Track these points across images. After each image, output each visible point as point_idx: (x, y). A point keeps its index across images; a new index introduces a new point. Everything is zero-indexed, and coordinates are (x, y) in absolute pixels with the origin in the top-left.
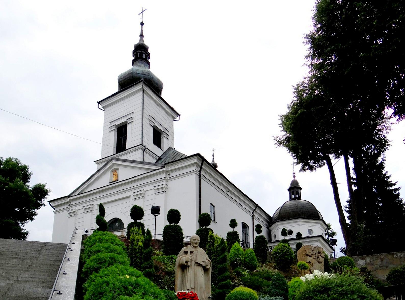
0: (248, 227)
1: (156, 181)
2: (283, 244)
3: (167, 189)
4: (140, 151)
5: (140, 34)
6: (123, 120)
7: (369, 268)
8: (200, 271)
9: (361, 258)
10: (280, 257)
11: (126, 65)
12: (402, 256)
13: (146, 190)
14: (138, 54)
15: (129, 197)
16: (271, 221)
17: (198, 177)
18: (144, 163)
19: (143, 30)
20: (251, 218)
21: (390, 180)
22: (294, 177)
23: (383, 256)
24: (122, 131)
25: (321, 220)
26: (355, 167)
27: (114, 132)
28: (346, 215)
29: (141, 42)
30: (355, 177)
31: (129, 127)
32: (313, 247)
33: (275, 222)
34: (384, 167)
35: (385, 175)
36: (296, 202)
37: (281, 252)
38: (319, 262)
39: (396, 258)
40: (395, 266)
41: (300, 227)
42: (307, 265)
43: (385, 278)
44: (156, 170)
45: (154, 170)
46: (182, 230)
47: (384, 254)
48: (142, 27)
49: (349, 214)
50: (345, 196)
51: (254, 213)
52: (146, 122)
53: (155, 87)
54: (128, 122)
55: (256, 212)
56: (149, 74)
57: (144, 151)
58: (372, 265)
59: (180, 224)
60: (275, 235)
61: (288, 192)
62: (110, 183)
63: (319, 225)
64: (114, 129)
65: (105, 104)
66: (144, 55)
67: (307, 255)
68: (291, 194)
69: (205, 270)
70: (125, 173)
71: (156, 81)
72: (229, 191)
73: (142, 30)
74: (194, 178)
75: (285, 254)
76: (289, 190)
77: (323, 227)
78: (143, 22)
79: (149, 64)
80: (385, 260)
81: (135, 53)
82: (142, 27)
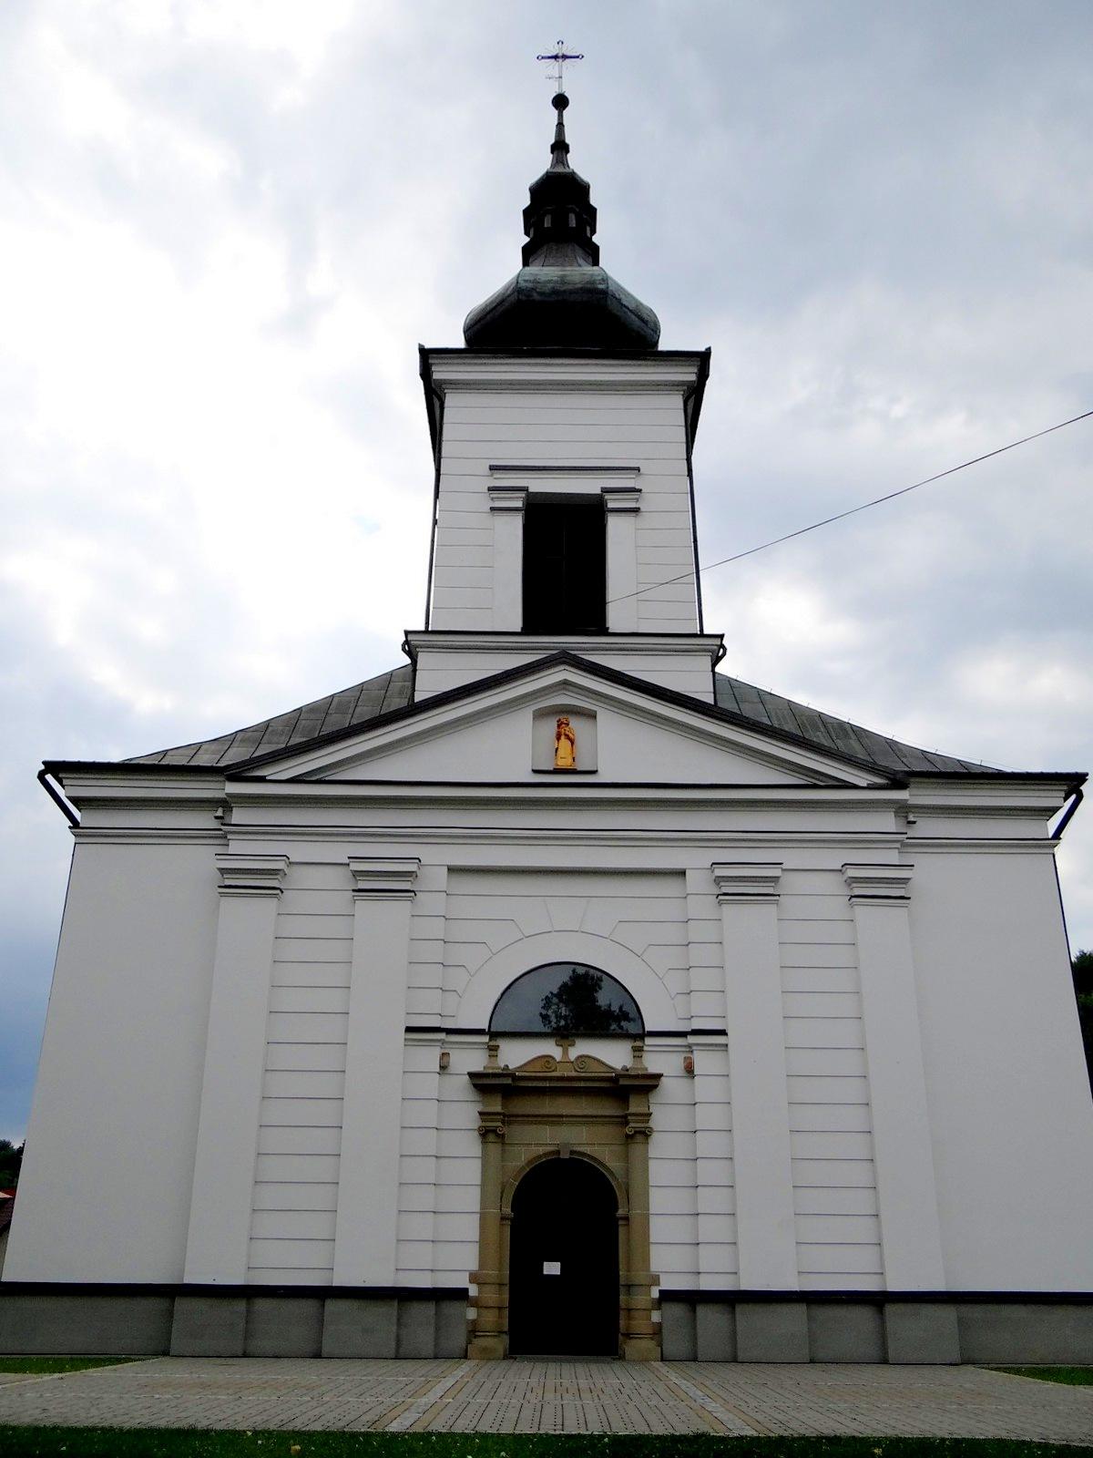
3: (405, 1039)
5: (553, 141)
11: (498, 263)
13: (291, 860)
19: (565, 123)
29: (560, 169)
44: (855, 787)
48: (560, 116)
62: (535, 771)
73: (560, 125)
82: (560, 116)
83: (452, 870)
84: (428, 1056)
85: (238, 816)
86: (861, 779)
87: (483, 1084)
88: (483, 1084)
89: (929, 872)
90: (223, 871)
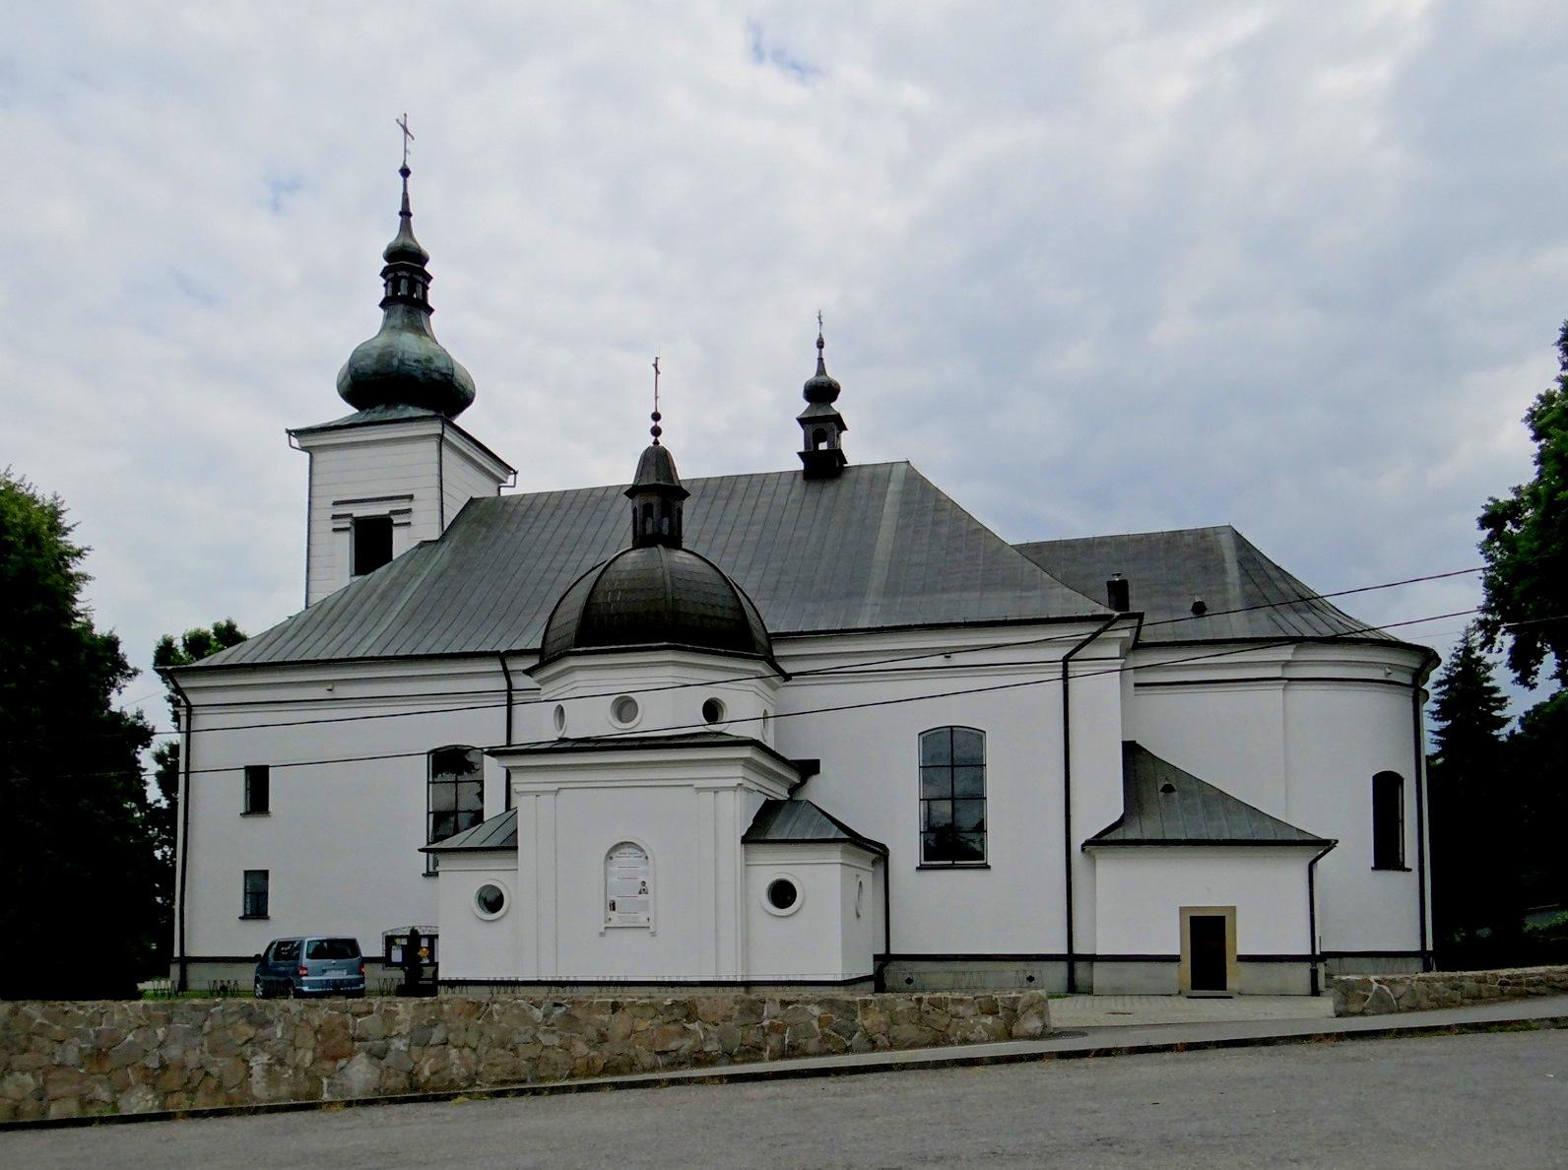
5: (400, 209)
6: (382, 510)
14: (403, 284)
22: (656, 432)
45: (342, 592)
56: (453, 376)
64: (348, 525)
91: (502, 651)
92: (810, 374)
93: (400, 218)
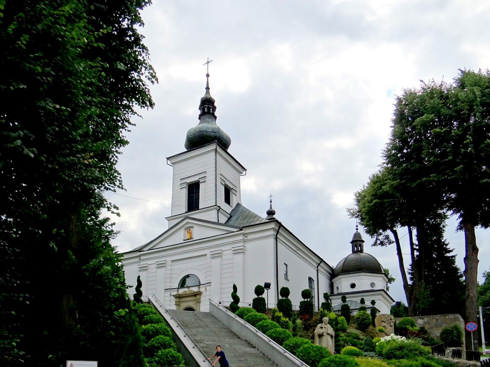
0: (314, 281)
1: (234, 242)
2: (363, 312)
3: (244, 250)
4: (215, 212)
5: (206, 87)
7: (427, 328)
8: (329, 337)
9: (420, 318)
10: (361, 321)
12: (453, 317)
15: (206, 255)
16: (333, 274)
17: (275, 240)
18: (218, 223)
20: (316, 272)
21: (448, 247)
22: (357, 229)
23: (438, 317)
24: (193, 189)
25: (383, 274)
26: (417, 234)
27: (185, 189)
28: (408, 276)
30: (417, 243)
31: (201, 185)
32: (387, 316)
33: (338, 275)
34: (443, 237)
35: (444, 242)
36: (359, 256)
37: (362, 318)
38: (391, 326)
39: (448, 319)
40: (446, 325)
41: (363, 281)
42: (384, 329)
43: (439, 335)
46: (291, 302)
47: (439, 316)
49: (411, 275)
50: (408, 261)
51: (319, 267)
52: (219, 181)
53: (223, 143)
54: (200, 182)
55: (321, 266)
56: (219, 132)
57: (218, 211)
58: (429, 323)
59: (289, 297)
60: (338, 288)
61: (351, 245)
62: (184, 240)
63: (381, 278)
64: (185, 186)
65: (175, 160)
66: (211, 109)
67: (383, 321)
68: (354, 246)
69: (332, 336)
70: (198, 233)
71: (225, 138)
72: (299, 249)
74: (272, 240)
75: (365, 319)
76: (351, 243)
77: (385, 280)
78: (209, 74)
79: (215, 118)
80: (439, 320)
81: (202, 107)
83: (172, 261)
84: (168, 294)
85: (142, 258)
86: (235, 230)
87: (176, 297)
88: (176, 297)
89: (249, 246)
90: (140, 268)
91: (141, 289)
92: (268, 209)
93: (205, 90)
